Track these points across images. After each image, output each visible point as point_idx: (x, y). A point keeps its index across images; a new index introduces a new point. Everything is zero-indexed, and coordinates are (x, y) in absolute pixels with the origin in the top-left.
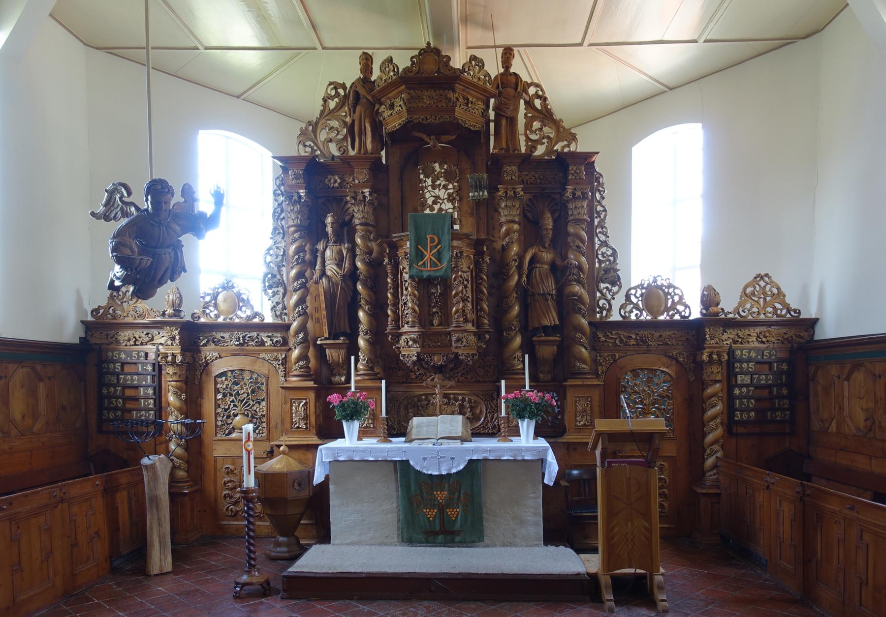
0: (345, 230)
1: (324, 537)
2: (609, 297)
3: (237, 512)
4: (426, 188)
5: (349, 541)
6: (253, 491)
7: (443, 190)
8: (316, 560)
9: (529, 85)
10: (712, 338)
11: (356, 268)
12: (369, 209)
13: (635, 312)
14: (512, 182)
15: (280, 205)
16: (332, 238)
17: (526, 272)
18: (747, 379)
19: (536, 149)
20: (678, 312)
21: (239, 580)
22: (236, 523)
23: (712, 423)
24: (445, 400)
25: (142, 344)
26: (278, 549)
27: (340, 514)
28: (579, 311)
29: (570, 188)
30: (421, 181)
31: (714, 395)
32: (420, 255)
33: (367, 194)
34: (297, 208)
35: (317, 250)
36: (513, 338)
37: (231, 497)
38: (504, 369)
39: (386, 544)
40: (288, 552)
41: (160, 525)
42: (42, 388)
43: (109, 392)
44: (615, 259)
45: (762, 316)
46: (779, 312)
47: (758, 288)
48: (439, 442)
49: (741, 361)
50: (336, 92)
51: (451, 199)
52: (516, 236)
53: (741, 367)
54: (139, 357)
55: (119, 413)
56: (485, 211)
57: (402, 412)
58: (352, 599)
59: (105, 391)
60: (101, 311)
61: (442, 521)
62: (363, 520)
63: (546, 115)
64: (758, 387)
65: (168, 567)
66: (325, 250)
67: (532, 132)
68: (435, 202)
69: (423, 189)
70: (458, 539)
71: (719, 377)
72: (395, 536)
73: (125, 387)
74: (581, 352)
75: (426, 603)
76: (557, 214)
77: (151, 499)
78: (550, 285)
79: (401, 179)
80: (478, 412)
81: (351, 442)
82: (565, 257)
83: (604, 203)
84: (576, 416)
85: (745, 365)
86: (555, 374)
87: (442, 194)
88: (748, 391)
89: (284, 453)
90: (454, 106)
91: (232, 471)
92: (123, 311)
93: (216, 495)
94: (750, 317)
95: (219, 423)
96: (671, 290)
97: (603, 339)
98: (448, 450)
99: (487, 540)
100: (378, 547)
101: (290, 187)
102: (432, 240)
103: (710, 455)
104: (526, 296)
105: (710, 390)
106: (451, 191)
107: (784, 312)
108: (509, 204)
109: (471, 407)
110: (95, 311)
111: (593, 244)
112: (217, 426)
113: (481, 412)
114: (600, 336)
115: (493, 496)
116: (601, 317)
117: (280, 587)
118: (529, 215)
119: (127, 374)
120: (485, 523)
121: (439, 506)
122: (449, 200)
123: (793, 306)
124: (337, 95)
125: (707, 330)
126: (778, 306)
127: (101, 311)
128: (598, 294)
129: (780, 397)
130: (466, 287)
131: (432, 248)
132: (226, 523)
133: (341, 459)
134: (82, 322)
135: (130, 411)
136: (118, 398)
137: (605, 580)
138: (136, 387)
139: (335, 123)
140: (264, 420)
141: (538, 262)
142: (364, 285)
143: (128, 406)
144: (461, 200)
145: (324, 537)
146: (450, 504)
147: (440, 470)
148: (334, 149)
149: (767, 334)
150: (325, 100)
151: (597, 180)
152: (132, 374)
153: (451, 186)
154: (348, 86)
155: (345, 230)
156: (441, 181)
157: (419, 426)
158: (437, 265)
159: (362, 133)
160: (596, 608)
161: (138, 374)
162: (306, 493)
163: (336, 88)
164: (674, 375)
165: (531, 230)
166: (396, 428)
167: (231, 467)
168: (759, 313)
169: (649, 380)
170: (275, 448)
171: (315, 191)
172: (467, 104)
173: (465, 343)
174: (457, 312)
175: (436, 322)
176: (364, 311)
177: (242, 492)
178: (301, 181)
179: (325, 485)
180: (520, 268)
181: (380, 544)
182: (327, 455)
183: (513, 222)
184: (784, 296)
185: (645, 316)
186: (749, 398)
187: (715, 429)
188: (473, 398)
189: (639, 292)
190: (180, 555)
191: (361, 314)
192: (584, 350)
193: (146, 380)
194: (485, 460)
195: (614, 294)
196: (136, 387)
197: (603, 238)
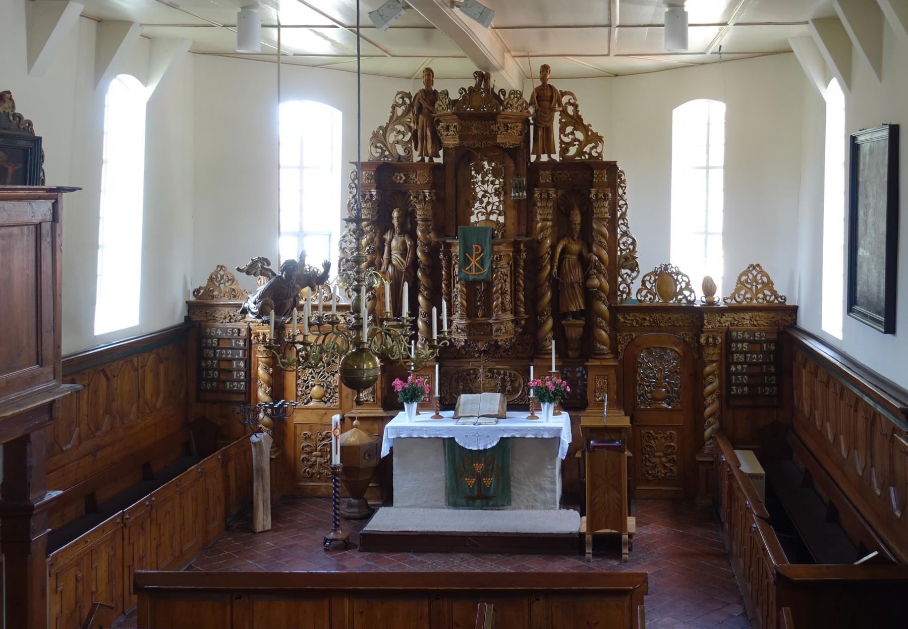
0: (408, 217)
1: (388, 501)
2: (629, 281)
3: (313, 474)
4: (477, 183)
6: (339, 468)
7: (491, 186)
8: (384, 521)
9: (563, 94)
10: (709, 323)
11: (417, 258)
12: (429, 207)
13: (649, 296)
14: (546, 185)
15: (354, 197)
16: (397, 230)
17: (556, 264)
18: (741, 358)
19: (568, 151)
20: (685, 297)
21: (328, 537)
22: (312, 484)
23: (709, 398)
24: (490, 374)
25: (236, 321)
26: (351, 510)
27: (401, 482)
28: (600, 299)
29: (593, 191)
30: (473, 177)
31: (712, 373)
32: (467, 262)
33: (427, 194)
34: (369, 205)
35: (384, 240)
36: (545, 322)
37: (308, 460)
38: (537, 352)
39: (436, 507)
40: (359, 512)
41: (264, 491)
42: (162, 367)
43: (207, 365)
44: (634, 248)
45: (755, 301)
46: (768, 298)
47: (751, 277)
48: (480, 419)
49: (737, 341)
50: (403, 101)
51: (497, 193)
52: (550, 230)
53: (737, 347)
54: (233, 333)
55: (215, 384)
56: (523, 211)
57: (454, 384)
58: (409, 552)
59: (203, 364)
60: (202, 291)
61: (479, 488)
63: (577, 121)
64: (750, 364)
65: (269, 527)
66: (391, 240)
67: (565, 135)
68: (484, 196)
69: (475, 183)
70: (491, 503)
71: (715, 358)
73: (221, 360)
74: (601, 335)
75: (461, 555)
76: (585, 208)
77: (258, 471)
78: (577, 274)
79: (456, 177)
80: (517, 385)
81: (409, 420)
82: (590, 250)
83: (625, 197)
84: (595, 392)
85: (740, 345)
86: (578, 353)
87: (491, 188)
88: (743, 368)
89: (356, 426)
90: (496, 135)
91: (309, 437)
92: (220, 292)
93: (295, 458)
94: (745, 302)
95: (299, 393)
96: (680, 277)
97: (622, 320)
98: (485, 429)
99: (513, 504)
100: (430, 510)
101: (364, 186)
102: (477, 249)
103: (708, 426)
104: (557, 285)
105: (708, 369)
106: (498, 186)
107: (773, 298)
108: (543, 204)
109: (512, 381)
110: (197, 291)
111: (616, 233)
112: (297, 396)
113: (520, 385)
114: (620, 317)
115: (519, 468)
116: (622, 299)
117: (357, 542)
118: (562, 208)
119: (222, 349)
120: (512, 490)
121: (479, 475)
122: (496, 195)
123: (780, 293)
124: (404, 103)
125: (705, 316)
126: (767, 292)
127: (202, 291)
128: (620, 279)
129: (770, 374)
130: (505, 281)
131: (477, 256)
132: (303, 484)
133: (403, 436)
134: (187, 302)
135: (224, 382)
136: (214, 370)
137: (589, 538)
138: (230, 361)
139: (400, 128)
140: (337, 390)
141: (568, 253)
142: (423, 273)
143: (222, 377)
144: (505, 193)
145: (388, 501)
146: (485, 474)
148: (400, 150)
149: (758, 318)
150: (394, 107)
151: (620, 176)
152: (227, 349)
153: (497, 182)
154: (413, 95)
155: (408, 217)
156: (490, 177)
157: (465, 404)
158: (480, 270)
159: (424, 138)
160: (580, 559)
161: (232, 349)
162: (374, 463)
163: (402, 98)
164: (681, 354)
165: (563, 229)
166: (448, 403)
167: (309, 433)
168: (751, 299)
169: (661, 357)
170: (347, 420)
171: (382, 192)
172: (507, 130)
173: (504, 325)
174: (496, 306)
175: (480, 314)
176: (423, 296)
177: (332, 468)
178: (373, 181)
179: (390, 457)
180: (552, 259)
181: (431, 507)
182: (392, 433)
183: (548, 220)
184: (773, 284)
185: (658, 300)
186: (743, 374)
187: (712, 403)
188: (514, 372)
189: (653, 278)
190: (275, 517)
191: (420, 298)
192: (603, 333)
193: (239, 354)
194: (513, 438)
195: (633, 279)
196: (230, 361)
197: (624, 228)
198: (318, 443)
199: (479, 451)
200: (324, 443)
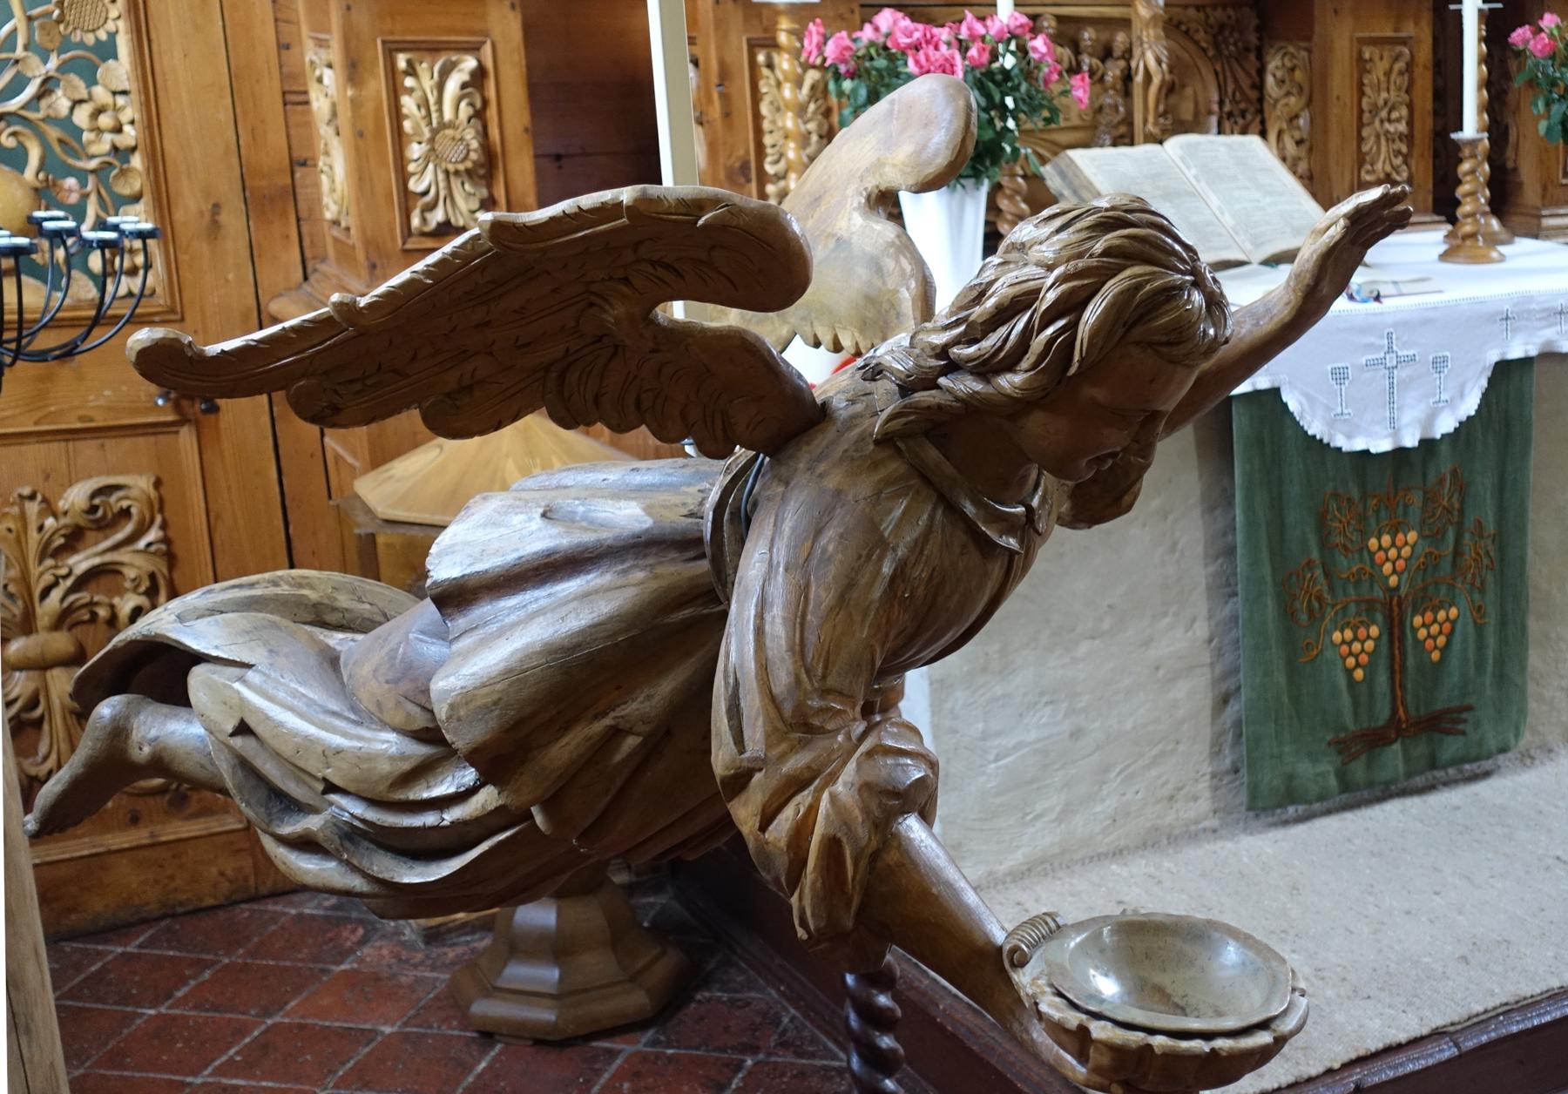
5: (1017, 858)
40: (559, 997)
61: (1396, 669)
62: (1076, 734)
70: (1451, 747)
72: (1204, 785)
147: (1396, 431)
198: (41, 573)
199: (1400, 453)
200: (81, 562)
